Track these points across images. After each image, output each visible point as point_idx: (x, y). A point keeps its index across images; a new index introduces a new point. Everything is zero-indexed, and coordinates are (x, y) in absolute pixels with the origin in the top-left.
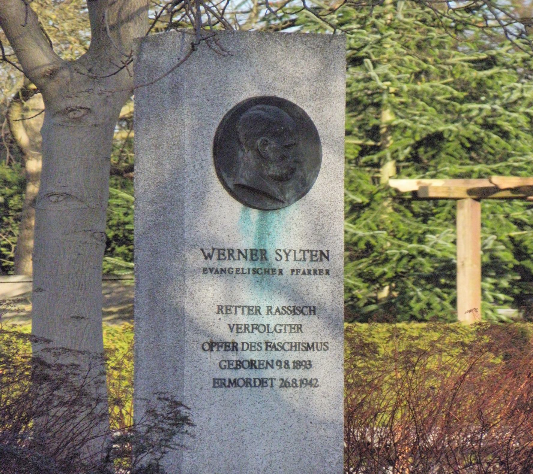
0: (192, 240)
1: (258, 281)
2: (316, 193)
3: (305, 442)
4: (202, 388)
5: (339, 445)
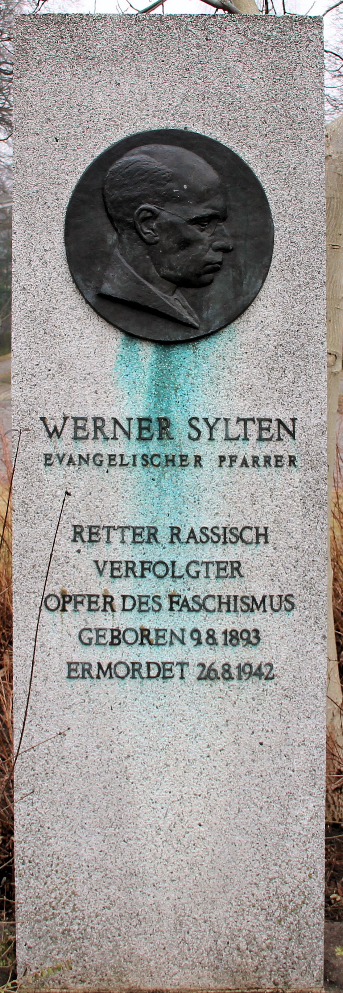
0: (25, 401)
1: (153, 480)
2: (270, 309)
3: (248, 778)
4: (46, 679)
5: (315, 784)
